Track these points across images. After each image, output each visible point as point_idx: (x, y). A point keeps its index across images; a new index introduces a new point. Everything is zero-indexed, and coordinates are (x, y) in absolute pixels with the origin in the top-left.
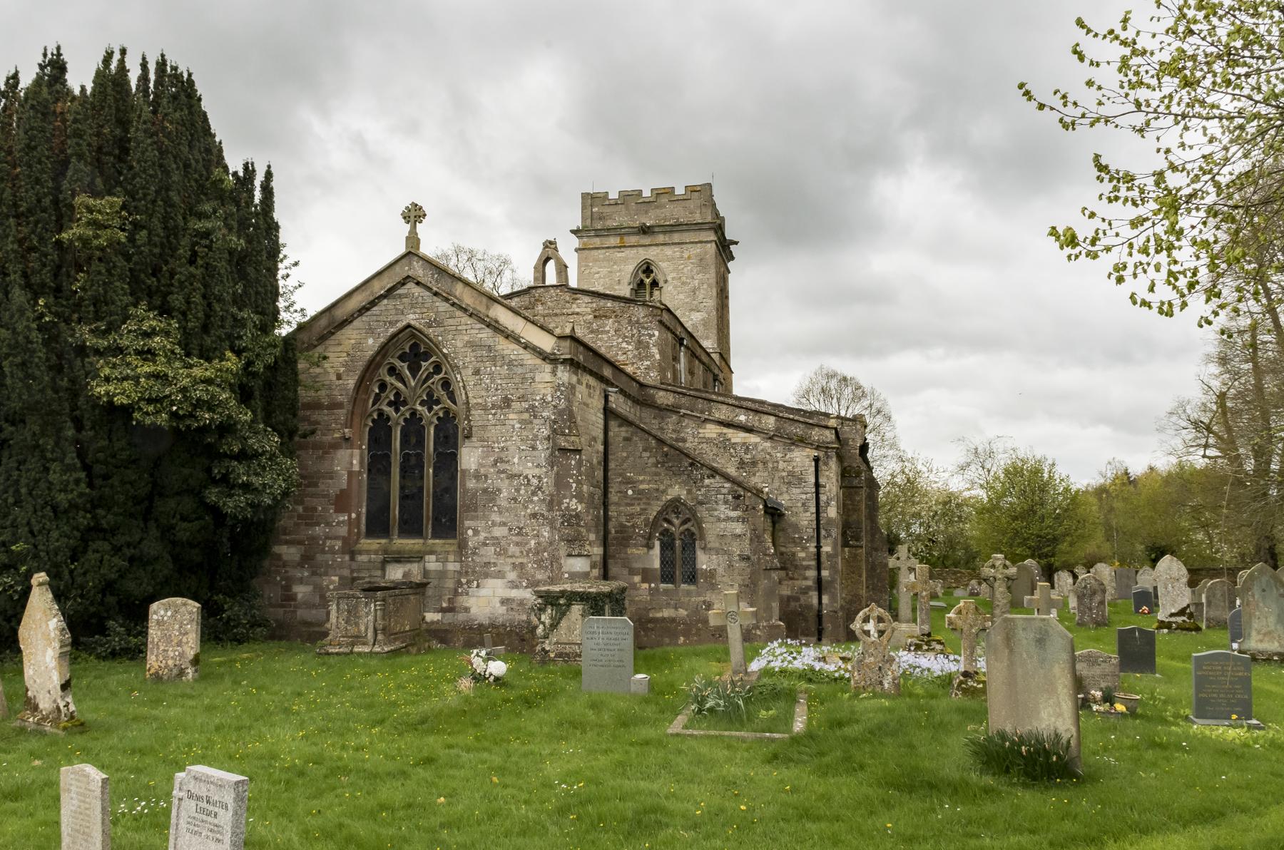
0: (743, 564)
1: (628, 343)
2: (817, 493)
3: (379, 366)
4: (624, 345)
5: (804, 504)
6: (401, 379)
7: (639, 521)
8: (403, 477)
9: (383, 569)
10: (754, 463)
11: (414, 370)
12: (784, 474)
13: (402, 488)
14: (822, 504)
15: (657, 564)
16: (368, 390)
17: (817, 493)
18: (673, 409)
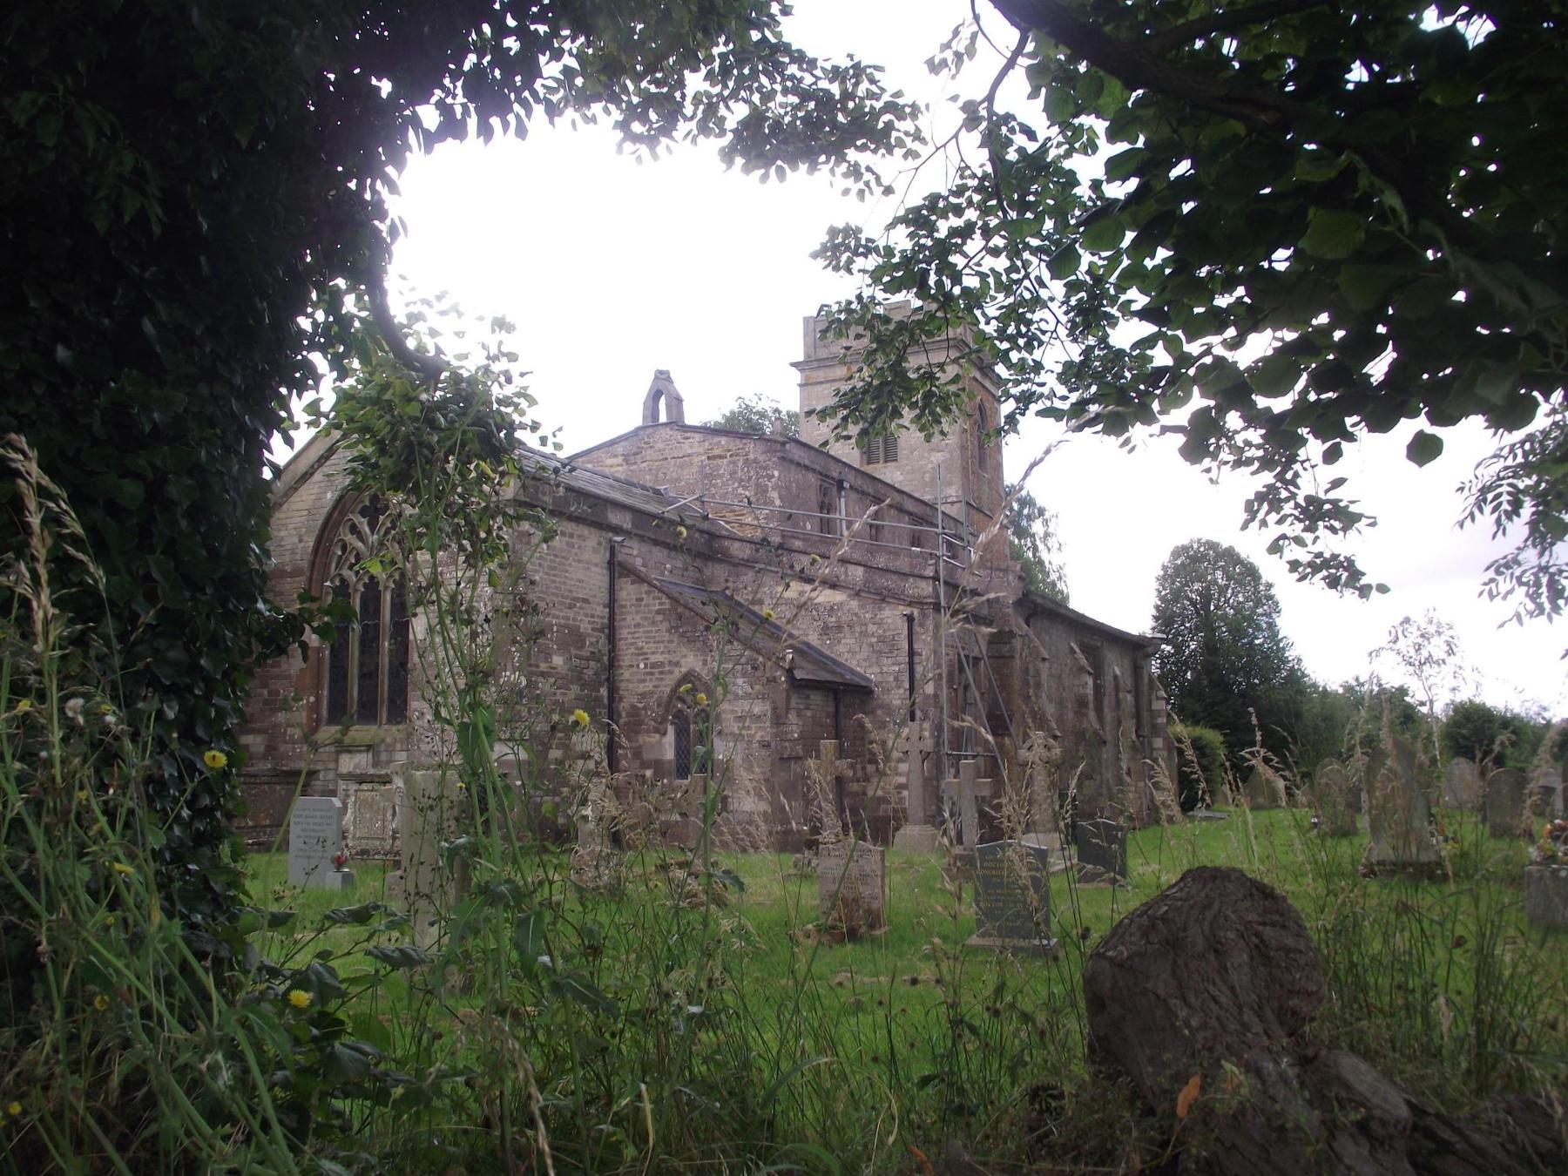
0: (763, 752)
1: (745, 488)
2: (911, 664)
3: (338, 524)
4: (740, 491)
5: (896, 679)
6: (361, 538)
7: (652, 702)
8: (362, 653)
9: (337, 762)
10: (839, 628)
11: (373, 526)
12: (874, 640)
13: (361, 665)
14: (917, 676)
15: (669, 754)
16: (328, 551)
17: (911, 664)
18: (748, 564)
